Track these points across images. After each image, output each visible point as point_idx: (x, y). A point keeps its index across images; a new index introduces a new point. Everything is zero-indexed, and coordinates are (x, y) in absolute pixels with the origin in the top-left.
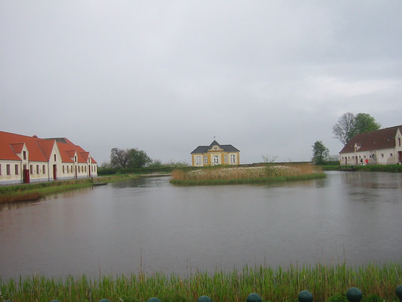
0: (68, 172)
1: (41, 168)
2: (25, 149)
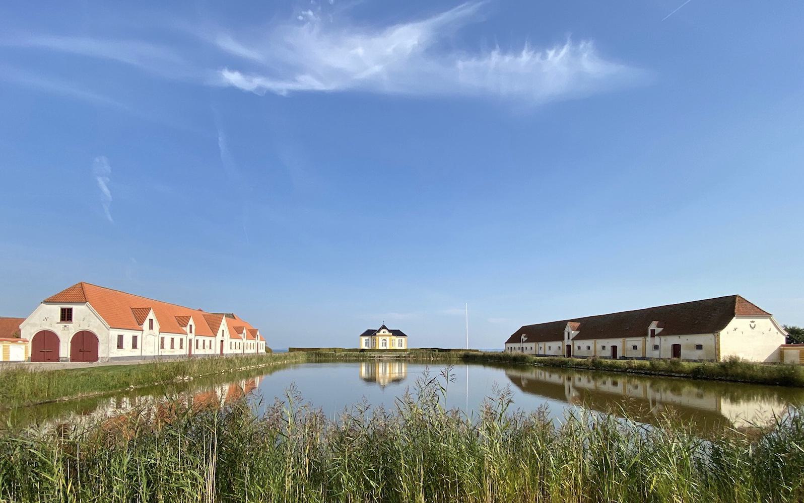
0: (235, 348)
1: (207, 343)
2: (191, 322)
